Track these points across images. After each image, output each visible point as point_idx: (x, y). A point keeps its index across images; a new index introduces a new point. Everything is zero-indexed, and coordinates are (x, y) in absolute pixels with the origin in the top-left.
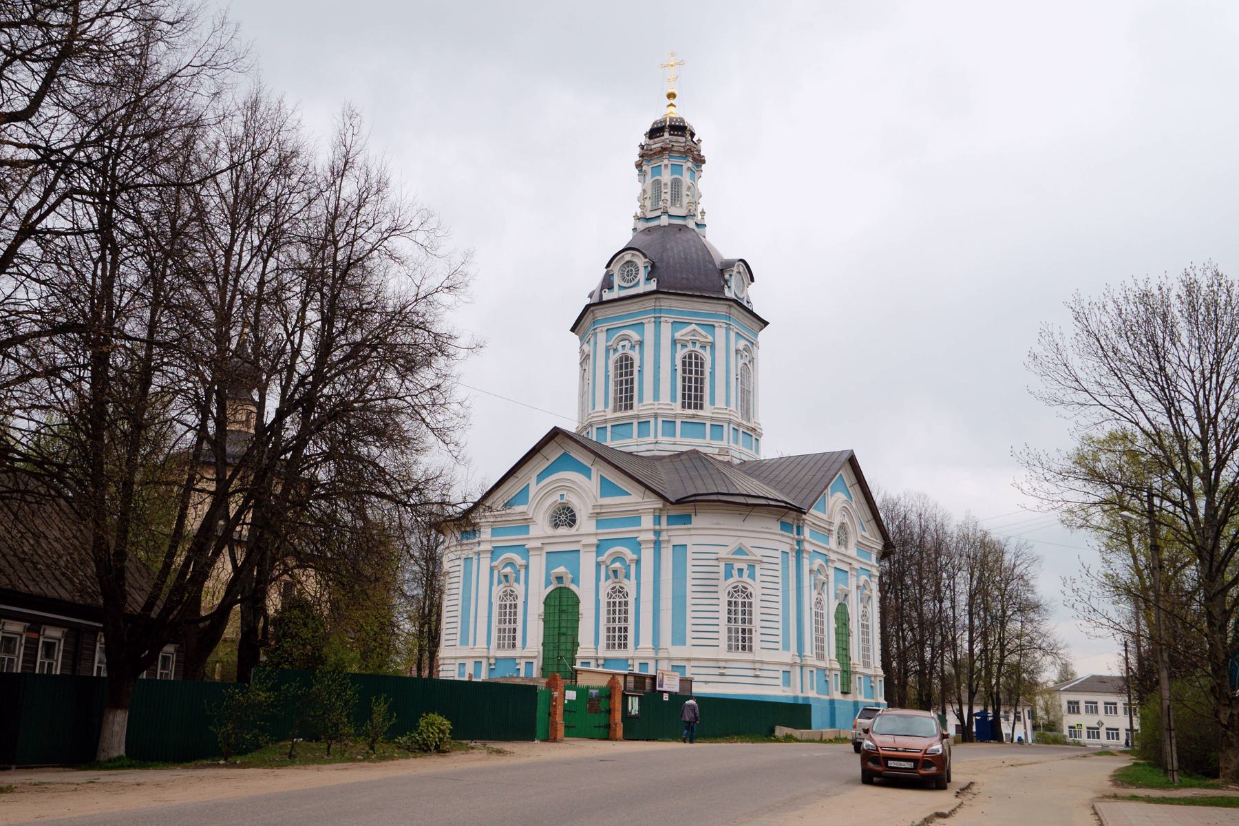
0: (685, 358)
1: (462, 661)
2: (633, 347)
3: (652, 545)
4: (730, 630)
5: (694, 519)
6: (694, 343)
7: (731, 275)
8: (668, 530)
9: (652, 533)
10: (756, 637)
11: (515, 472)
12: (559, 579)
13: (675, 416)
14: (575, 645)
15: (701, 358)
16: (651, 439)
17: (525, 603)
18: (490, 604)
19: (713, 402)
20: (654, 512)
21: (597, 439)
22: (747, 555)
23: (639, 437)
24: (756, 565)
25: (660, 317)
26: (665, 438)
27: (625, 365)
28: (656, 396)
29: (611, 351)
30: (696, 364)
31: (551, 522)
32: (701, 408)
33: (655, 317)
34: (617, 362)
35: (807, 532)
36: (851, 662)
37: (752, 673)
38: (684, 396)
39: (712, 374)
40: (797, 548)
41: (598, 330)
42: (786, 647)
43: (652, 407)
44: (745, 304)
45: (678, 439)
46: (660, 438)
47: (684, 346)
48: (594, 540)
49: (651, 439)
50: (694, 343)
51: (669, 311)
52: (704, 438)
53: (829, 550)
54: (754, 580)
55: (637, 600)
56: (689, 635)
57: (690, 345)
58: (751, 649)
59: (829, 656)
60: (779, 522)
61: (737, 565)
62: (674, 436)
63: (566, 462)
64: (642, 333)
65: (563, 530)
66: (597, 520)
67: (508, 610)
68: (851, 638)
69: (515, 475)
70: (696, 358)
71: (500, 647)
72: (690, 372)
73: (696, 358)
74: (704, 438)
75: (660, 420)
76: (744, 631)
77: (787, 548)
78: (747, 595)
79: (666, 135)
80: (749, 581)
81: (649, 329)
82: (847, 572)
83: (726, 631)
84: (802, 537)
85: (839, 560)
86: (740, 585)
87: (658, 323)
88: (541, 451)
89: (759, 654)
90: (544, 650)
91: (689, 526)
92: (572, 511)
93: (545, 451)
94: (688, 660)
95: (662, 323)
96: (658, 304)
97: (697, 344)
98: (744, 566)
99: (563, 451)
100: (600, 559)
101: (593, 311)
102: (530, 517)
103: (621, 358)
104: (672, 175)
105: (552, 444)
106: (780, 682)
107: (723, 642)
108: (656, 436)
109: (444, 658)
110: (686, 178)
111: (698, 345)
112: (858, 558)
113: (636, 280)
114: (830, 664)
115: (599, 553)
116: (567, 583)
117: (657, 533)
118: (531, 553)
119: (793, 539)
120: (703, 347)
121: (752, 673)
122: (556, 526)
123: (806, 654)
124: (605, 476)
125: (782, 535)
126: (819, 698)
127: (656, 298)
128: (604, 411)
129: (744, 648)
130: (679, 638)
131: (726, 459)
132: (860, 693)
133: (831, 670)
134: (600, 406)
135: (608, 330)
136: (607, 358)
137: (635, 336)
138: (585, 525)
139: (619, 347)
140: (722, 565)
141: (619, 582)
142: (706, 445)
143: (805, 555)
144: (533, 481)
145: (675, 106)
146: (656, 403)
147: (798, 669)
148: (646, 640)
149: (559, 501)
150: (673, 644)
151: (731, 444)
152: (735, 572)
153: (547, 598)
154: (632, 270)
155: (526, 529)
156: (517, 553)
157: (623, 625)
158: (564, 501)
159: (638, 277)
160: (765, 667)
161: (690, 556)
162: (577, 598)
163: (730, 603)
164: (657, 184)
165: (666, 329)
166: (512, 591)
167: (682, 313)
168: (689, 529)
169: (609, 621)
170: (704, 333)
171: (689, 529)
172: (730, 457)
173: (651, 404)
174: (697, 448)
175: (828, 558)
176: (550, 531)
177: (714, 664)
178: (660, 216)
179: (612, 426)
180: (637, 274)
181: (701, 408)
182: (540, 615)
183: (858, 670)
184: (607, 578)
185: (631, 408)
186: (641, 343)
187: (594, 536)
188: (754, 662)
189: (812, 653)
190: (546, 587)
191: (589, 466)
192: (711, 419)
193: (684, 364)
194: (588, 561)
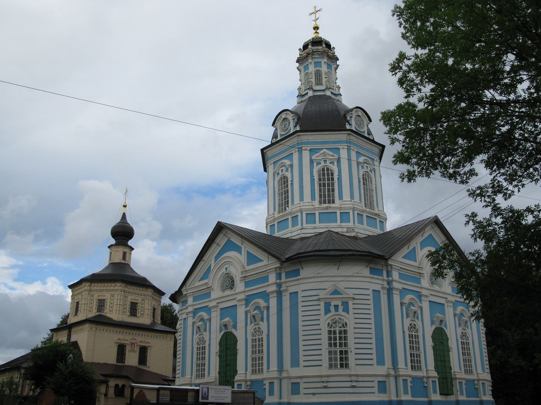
0: (320, 171)
2: (287, 170)
3: (275, 295)
4: (330, 352)
5: (301, 271)
6: (325, 161)
7: (351, 117)
8: (285, 282)
10: (351, 357)
11: (202, 257)
12: (225, 326)
13: (314, 209)
14: (236, 372)
16: (299, 226)
17: (209, 345)
18: (193, 347)
19: (341, 197)
20: (276, 271)
21: (270, 233)
22: (342, 294)
23: (293, 227)
24: (349, 301)
25: (302, 147)
26: (308, 225)
27: (284, 181)
28: (302, 198)
29: (276, 175)
30: (328, 174)
32: (333, 202)
34: (279, 181)
35: (395, 275)
36: (452, 371)
37: (349, 384)
39: (339, 179)
40: (388, 287)
42: (381, 361)
43: (299, 205)
44: (366, 135)
45: (317, 224)
46: (305, 225)
47: (318, 164)
48: (242, 296)
49: (299, 226)
50: (325, 161)
51: (308, 143)
52: (377, 228)
53: (421, 288)
54: (348, 313)
55: (268, 335)
56: (302, 358)
57: (322, 162)
58: (347, 366)
59: (476, 371)
60: (368, 268)
61: (333, 303)
62: (315, 223)
63: (230, 246)
64: (292, 160)
65: (228, 292)
66: (245, 282)
68: (451, 353)
72: (324, 179)
73: (328, 170)
76: (341, 352)
77: (378, 288)
80: (344, 314)
81: (296, 156)
82: (379, 291)
83: (327, 354)
84: (390, 279)
85: (431, 295)
86: (337, 317)
87: (300, 150)
88: (215, 241)
89: (354, 369)
90: (219, 377)
91: (298, 277)
92: (232, 278)
93: (218, 240)
94: (301, 377)
95: (303, 151)
96: (300, 139)
98: (339, 303)
99: (227, 238)
102: (210, 286)
103: (281, 178)
105: (221, 236)
106: (376, 390)
107: (325, 362)
108: (302, 225)
111: (328, 162)
112: (400, 280)
113: (289, 129)
114: (478, 376)
115: (247, 305)
116: (230, 329)
117: (279, 285)
118: (212, 310)
119: (383, 280)
120: (332, 163)
121: (349, 384)
122: (223, 291)
123: (400, 366)
124: (251, 252)
125: (372, 278)
126: (413, 401)
129: (342, 366)
130: (295, 363)
131: (353, 234)
132: (462, 394)
133: (428, 378)
135: (274, 162)
136: (274, 180)
138: (240, 286)
139: (280, 172)
140: (322, 304)
141: (257, 324)
142: (338, 227)
143: (394, 292)
146: (301, 202)
147: (392, 380)
148: (274, 366)
149: (225, 272)
150: (292, 366)
151: (356, 224)
152: (332, 308)
153: (220, 340)
154: (287, 124)
155: (208, 295)
156: (205, 312)
157: (254, 356)
159: (290, 126)
160: (361, 379)
161: (300, 299)
162: (236, 338)
163: (330, 332)
164: (307, 74)
165: (306, 155)
167: (317, 143)
168: (298, 280)
170: (331, 154)
171: (298, 280)
172: (355, 233)
174: (331, 229)
175: (420, 294)
176: (221, 294)
177: (348, 379)
179: (278, 222)
181: (333, 202)
182: (217, 353)
183: (457, 376)
186: (291, 166)
187: (244, 293)
188: (350, 376)
189: (460, 369)
190: (220, 332)
192: (340, 208)
194: (241, 311)
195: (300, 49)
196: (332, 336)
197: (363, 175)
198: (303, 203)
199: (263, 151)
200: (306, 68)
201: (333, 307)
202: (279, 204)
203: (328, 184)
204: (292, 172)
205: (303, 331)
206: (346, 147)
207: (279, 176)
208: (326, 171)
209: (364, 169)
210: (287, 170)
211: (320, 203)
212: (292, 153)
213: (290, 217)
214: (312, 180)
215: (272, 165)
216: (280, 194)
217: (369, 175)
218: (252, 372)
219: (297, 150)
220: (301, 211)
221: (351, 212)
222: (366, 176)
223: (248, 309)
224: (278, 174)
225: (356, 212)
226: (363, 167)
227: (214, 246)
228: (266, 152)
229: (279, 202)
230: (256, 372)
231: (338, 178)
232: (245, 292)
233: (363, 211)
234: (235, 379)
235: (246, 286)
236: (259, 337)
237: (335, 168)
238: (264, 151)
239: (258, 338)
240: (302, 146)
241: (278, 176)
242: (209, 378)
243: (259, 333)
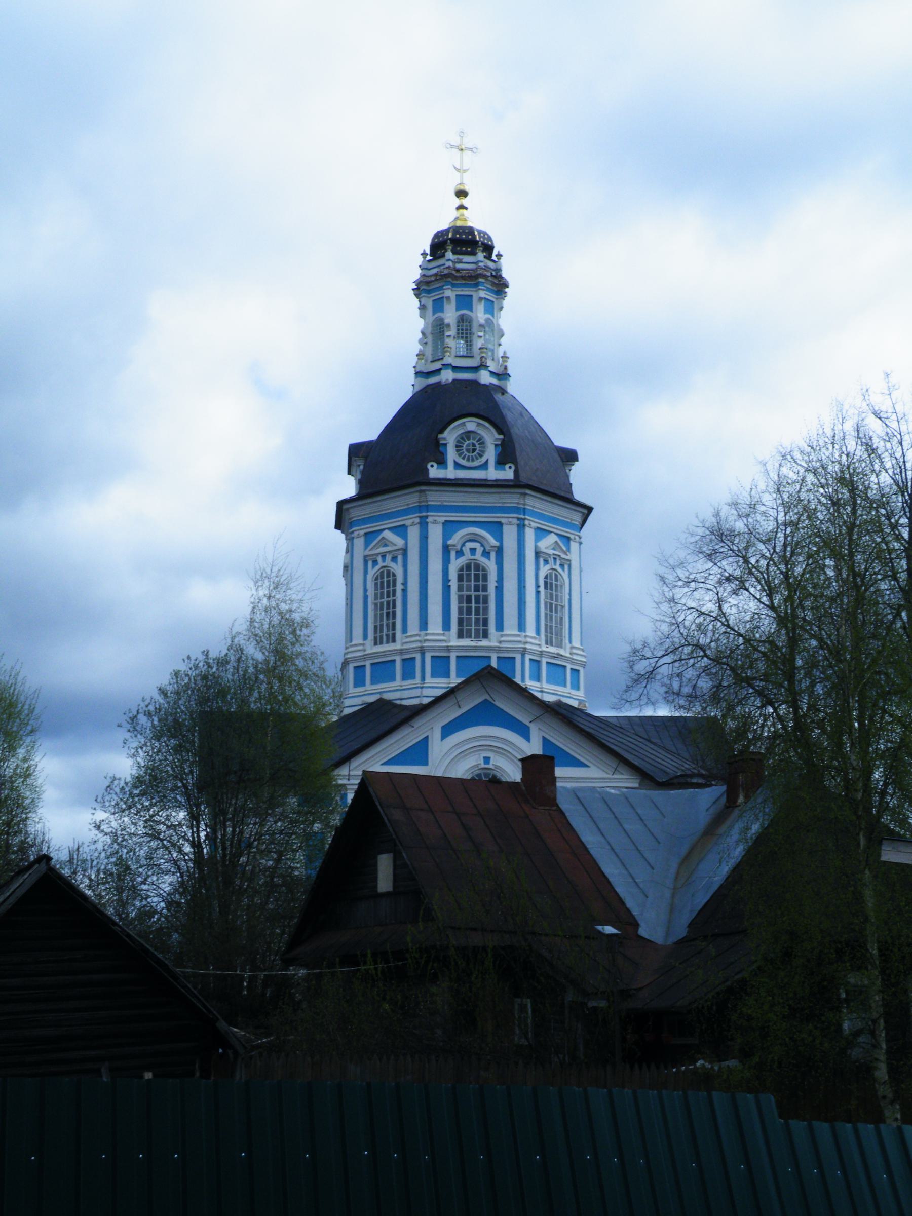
6: (384, 557)
13: (448, 649)
29: (370, 564)
32: (486, 635)
33: (420, 517)
34: (377, 579)
39: (499, 589)
41: (356, 534)
43: (418, 638)
47: (460, 553)
52: (565, 686)
74: (565, 686)
75: (428, 656)
79: (449, 255)
81: (414, 534)
87: (424, 525)
95: (430, 526)
103: (468, 567)
104: (457, 309)
110: (480, 314)
113: (484, 459)
127: (421, 491)
128: (363, 645)
134: (358, 638)
135: (366, 534)
136: (366, 572)
137: (399, 542)
139: (466, 550)
144: (437, 733)
145: (466, 208)
146: (423, 633)
149: (483, 766)
158: (490, 766)
165: (435, 534)
173: (416, 635)
174: (565, 700)
178: (440, 370)
180: (483, 452)
181: (486, 635)
185: (394, 641)
191: (527, 723)
193: (460, 578)
195: (424, 254)
196: (481, 628)
197: (546, 577)
198: (426, 635)
199: (341, 505)
200: (439, 305)
202: (376, 627)
203: (477, 610)
204: (405, 566)
206: (515, 521)
207: (377, 568)
208: (473, 630)
209: (548, 565)
210: (394, 559)
211: (460, 635)
212: (404, 525)
213: (398, 659)
214: (446, 588)
215: (362, 539)
216: (378, 607)
217: (559, 576)
219: (417, 520)
220: (422, 651)
221: (518, 657)
222: (551, 579)
224: (375, 562)
225: (528, 657)
226: (546, 562)
228: (348, 509)
229: (375, 621)
231: (496, 587)
233: (541, 653)
237: (491, 565)
238: (345, 507)
240: (429, 514)
241: (373, 567)
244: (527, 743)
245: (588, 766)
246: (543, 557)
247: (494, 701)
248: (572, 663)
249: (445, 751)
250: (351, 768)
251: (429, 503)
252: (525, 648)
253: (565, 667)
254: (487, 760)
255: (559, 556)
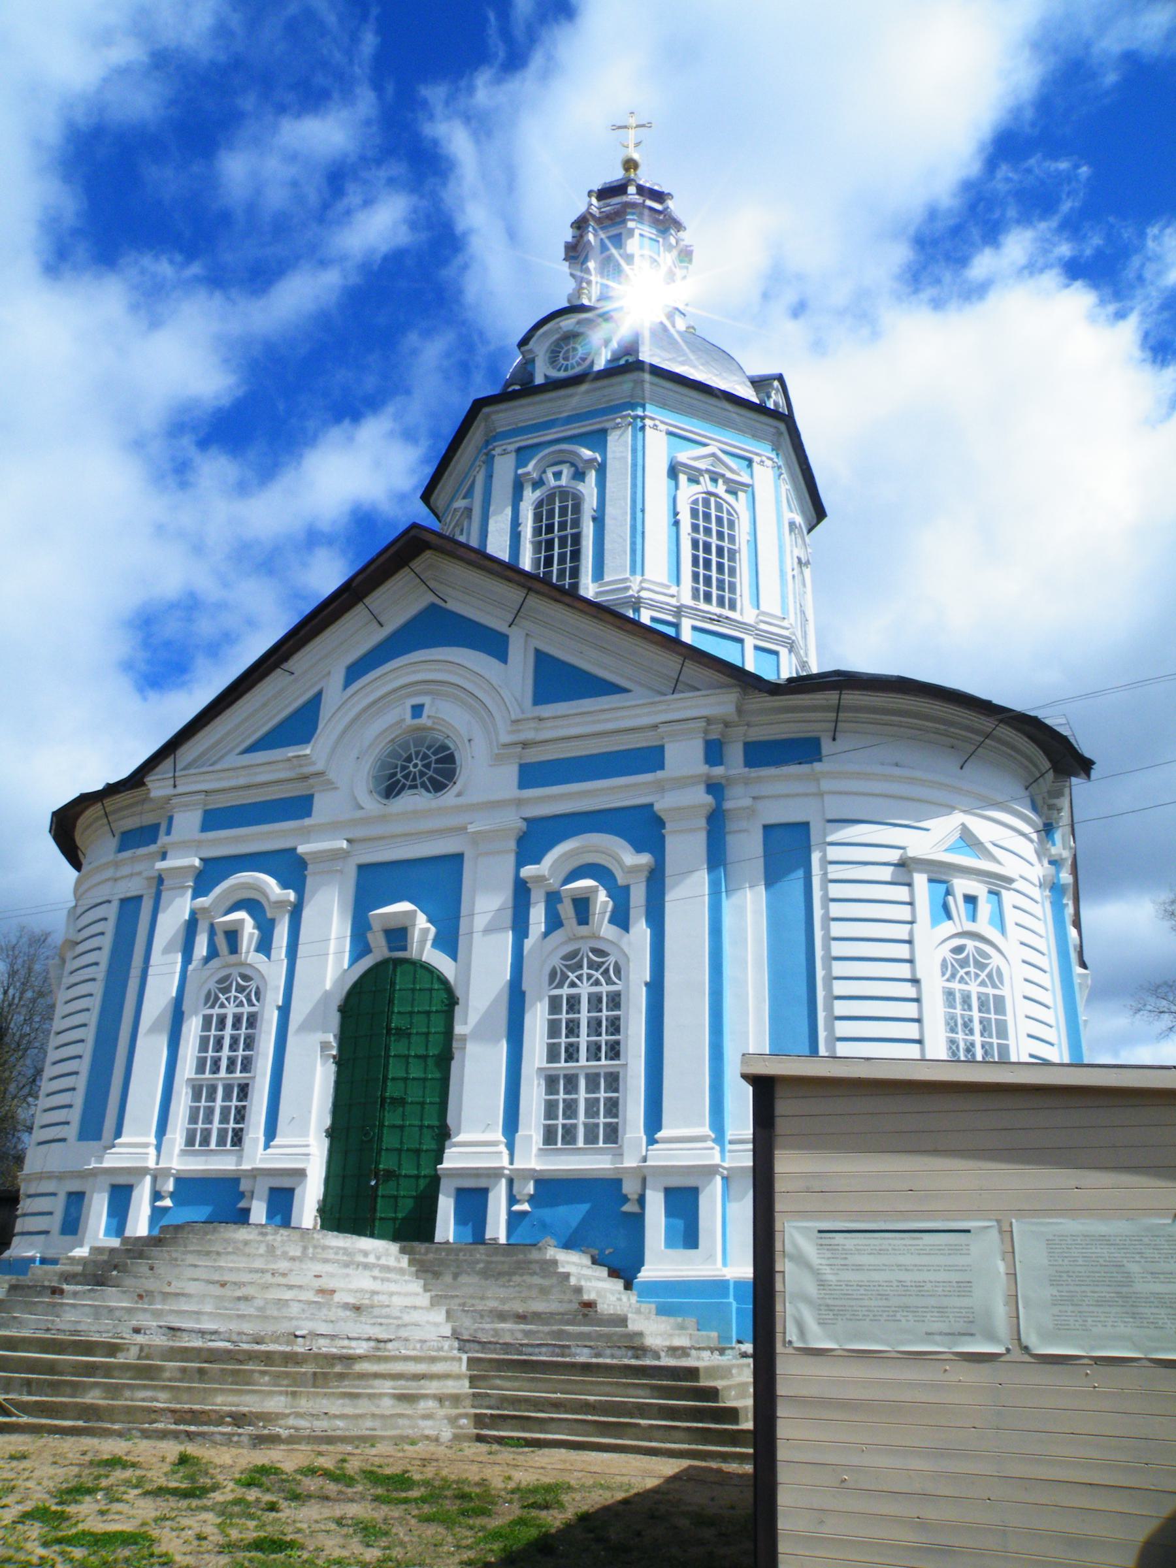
0: (696, 502)
1: (75, 1186)
9: (702, 788)
11: (286, 658)
15: (729, 513)
31: (377, 779)
38: (696, 576)
67: (228, 1031)
69: (286, 666)
70: (719, 508)
71: (196, 1140)
73: (719, 508)
78: (990, 976)
93: (378, 599)
97: (720, 481)
100: (528, 871)
101: (488, 415)
102: (319, 767)
103: (550, 498)
109: (41, 1176)
117: (715, 788)
152: (958, 906)
158: (424, 721)
166: (245, 978)
169: (553, 1056)
176: (372, 804)
184: (554, 923)
191: (502, 627)
193: (694, 513)
201: (960, 900)
205: (1024, 962)
218: (190, 1141)
223: (203, 901)
227: (355, 618)
230: (205, 1141)
232: (519, 802)
234: (446, 1165)
235: (524, 783)
236: (239, 1010)
239: (590, 995)
242: (269, 1151)
243: (242, 997)
244: (503, 665)
245: (625, 690)
246: (685, 473)
247: (446, 602)
248: (758, 636)
249: (344, 699)
250: (179, 767)
251: (498, 430)
252: (639, 598)
253: (740, 641)
254: (417, 710)
255: (723, 476)
